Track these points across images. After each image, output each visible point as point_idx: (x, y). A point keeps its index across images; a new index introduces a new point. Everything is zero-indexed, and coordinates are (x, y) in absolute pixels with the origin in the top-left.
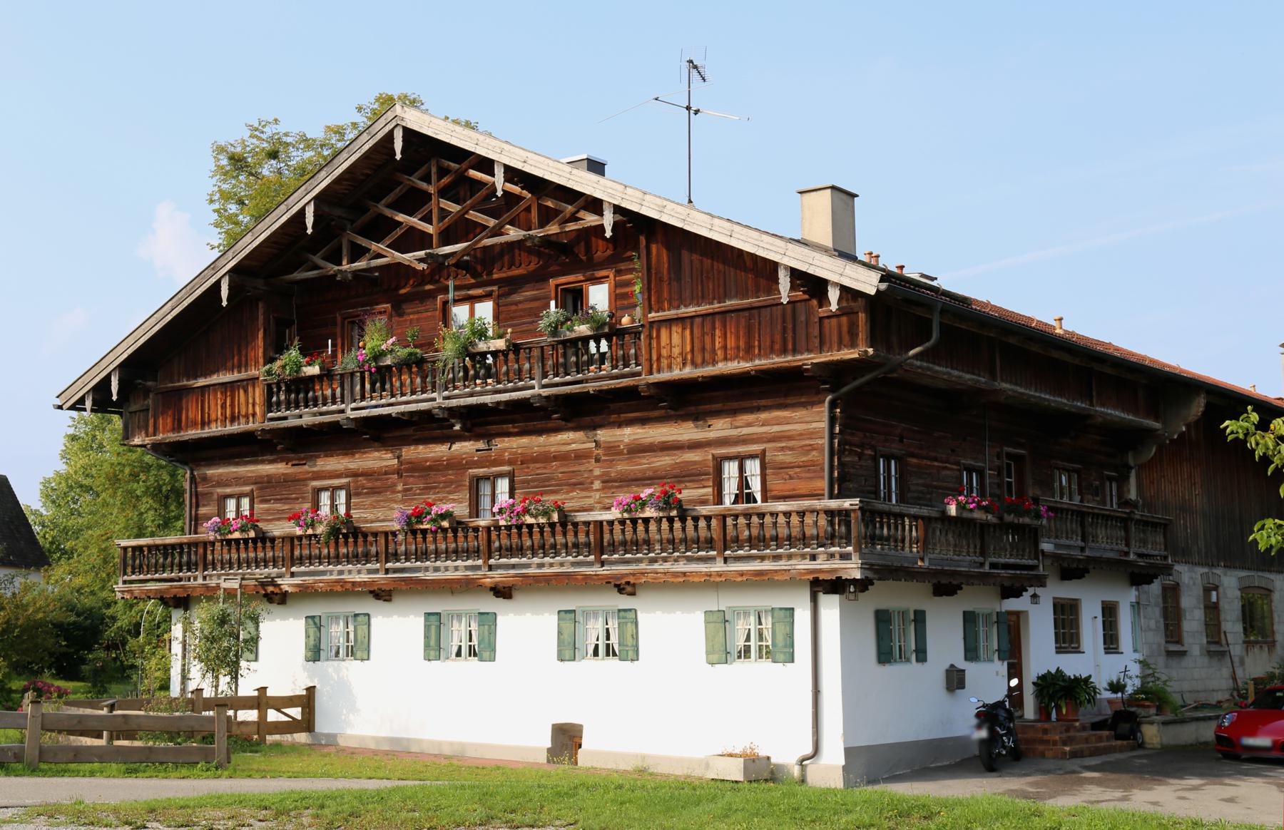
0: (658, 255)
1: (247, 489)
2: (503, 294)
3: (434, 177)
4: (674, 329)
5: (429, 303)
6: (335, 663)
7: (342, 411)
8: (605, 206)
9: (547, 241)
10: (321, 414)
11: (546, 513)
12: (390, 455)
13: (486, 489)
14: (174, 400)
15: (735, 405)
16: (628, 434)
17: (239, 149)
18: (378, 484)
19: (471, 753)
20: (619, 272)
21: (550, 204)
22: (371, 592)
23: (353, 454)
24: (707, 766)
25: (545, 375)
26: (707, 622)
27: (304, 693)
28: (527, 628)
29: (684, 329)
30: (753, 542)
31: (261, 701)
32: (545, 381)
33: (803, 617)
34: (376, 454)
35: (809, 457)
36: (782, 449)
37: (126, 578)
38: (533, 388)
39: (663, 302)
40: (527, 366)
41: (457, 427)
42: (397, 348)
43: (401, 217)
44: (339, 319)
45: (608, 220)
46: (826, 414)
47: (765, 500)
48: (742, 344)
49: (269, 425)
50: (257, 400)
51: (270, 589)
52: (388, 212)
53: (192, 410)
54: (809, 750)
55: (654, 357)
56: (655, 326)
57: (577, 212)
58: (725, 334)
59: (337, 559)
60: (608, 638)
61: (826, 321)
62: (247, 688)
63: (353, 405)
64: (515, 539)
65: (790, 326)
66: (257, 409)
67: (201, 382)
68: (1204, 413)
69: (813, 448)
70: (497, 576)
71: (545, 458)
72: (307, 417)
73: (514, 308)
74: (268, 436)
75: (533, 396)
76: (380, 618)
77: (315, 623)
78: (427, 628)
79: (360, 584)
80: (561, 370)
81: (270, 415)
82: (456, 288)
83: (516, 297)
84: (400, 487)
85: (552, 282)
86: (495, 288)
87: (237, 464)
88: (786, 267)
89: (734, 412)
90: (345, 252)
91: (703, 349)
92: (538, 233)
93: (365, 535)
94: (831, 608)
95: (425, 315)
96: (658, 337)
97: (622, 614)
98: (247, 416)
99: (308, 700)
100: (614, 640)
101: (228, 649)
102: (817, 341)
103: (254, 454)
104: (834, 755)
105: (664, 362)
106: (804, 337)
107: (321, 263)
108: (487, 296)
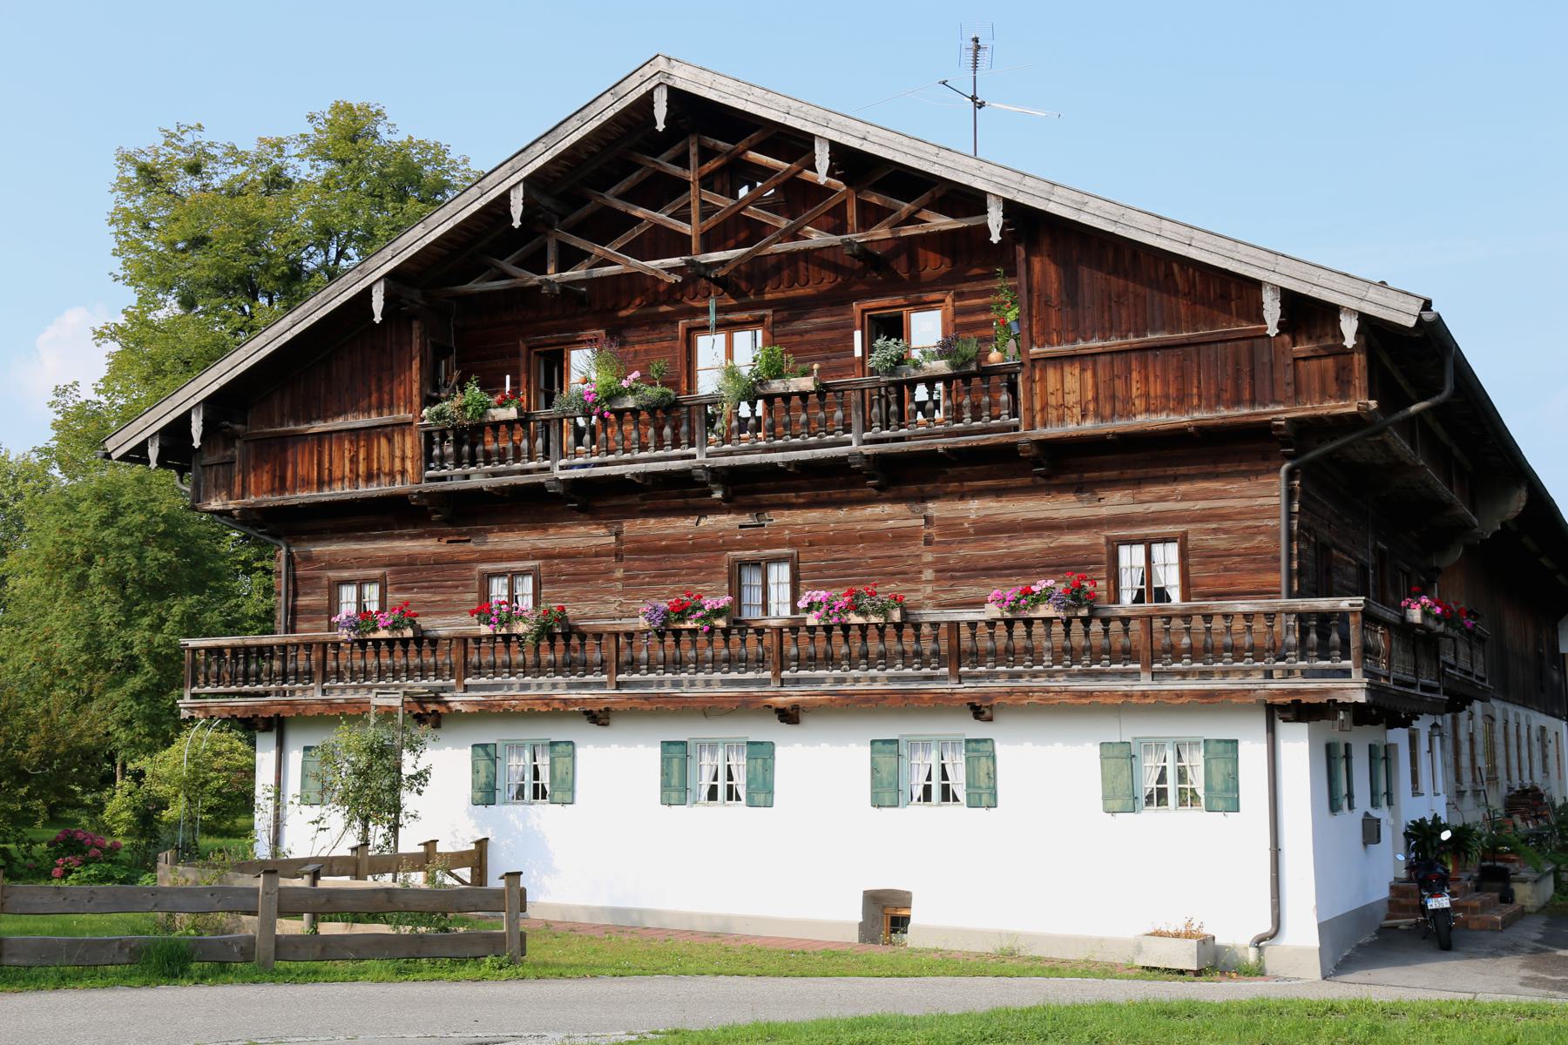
0: (1044, 273)
1: (377, 572)
2: (782, 321)
3: (693, 160)
4: (1067, 369)
5: (666, 330)
6: (520, 808)
7: (547, 469)
8: (991, 201)
9: (864, 253)
10: (494, 475)
11: (884, 611)
12: (603, 531)
13: (752, 578)
14: (273, 453)
15: (1141, 472)
16: (975, 509)
17: (149, 160)
18: (585, 568)
19: (739, 930)
20: (959, 296)
21: (875, 199)
22: (586, 713)
23: (545, 529)
24: (1139, 949)
25: (867, 427)
26: (1103, 757)
27: (473, 847)
28: (823, 767)
29: (1083, 370)
30: (1195, 653)
31: (427, 856)
32: (866, 435)
33: (1253, 752)
34: (582, 529)
35: (1255, 543)
36: (1215, 531)
37: (195, 690)
38: (849, 443)
39: (1049, 334)
40: (839, 414)
41: (718, 495)
42: (642, 386)
43: (640, 212)
44: (523, 347)
45: (995, 219)
46: (1283, 486)
47: (1186, 596)
48: (1172, 391)
49: (427, 487)
50: (409, 453)
51: (432, 707)
52: (621, 205)
53: (303, 464)
54: (1267, 927)
55: (1038, 406)
56: (1038, 365)
57: (918, 211)
58: (1147, 378)
59: (538, 668)
60: (536, 776)
61: (1301, 363)
62: (410, 842)
63: (563, 462)
64: (824, 645)
65: (1246, 369)
66: (409, 465)
67: (319, 427)
68: (1525, 508)
69: (1259, 531)
70: (790, 696)
71: (848, 539)
72: (479, 478)
73: (797, 339)
74: (425, 502)
75: (852, 454)
76: (590, 747)
77: (486, 754)
78: (666, 761)
79: (575, 702)
80: (893, 421)
81: (429, 473)
82: (718, 310)
83: (800, 325)
84: (619, 574)
85: (856, 307)
86: (769, 312)
87: (360, 539)
88: (1274, 287)
89: (1138, 482)
90: (551, 255)
91: (1113, 397)
92: (859, 237)
93: (583, 636)
94: (1297, 744)
95: (659, 345)
96: (1043, 379)
97: (972, 745)
98: (391, 474)
99: (478, 856)
100: (545, 778)
101: (377, 793)
102: (1290, 390)
103: (387, 527)
104: (1303, 932)
105: (1053, 414)
106: (1267, 383)
107: (514, 270)
108: (759, 322)
